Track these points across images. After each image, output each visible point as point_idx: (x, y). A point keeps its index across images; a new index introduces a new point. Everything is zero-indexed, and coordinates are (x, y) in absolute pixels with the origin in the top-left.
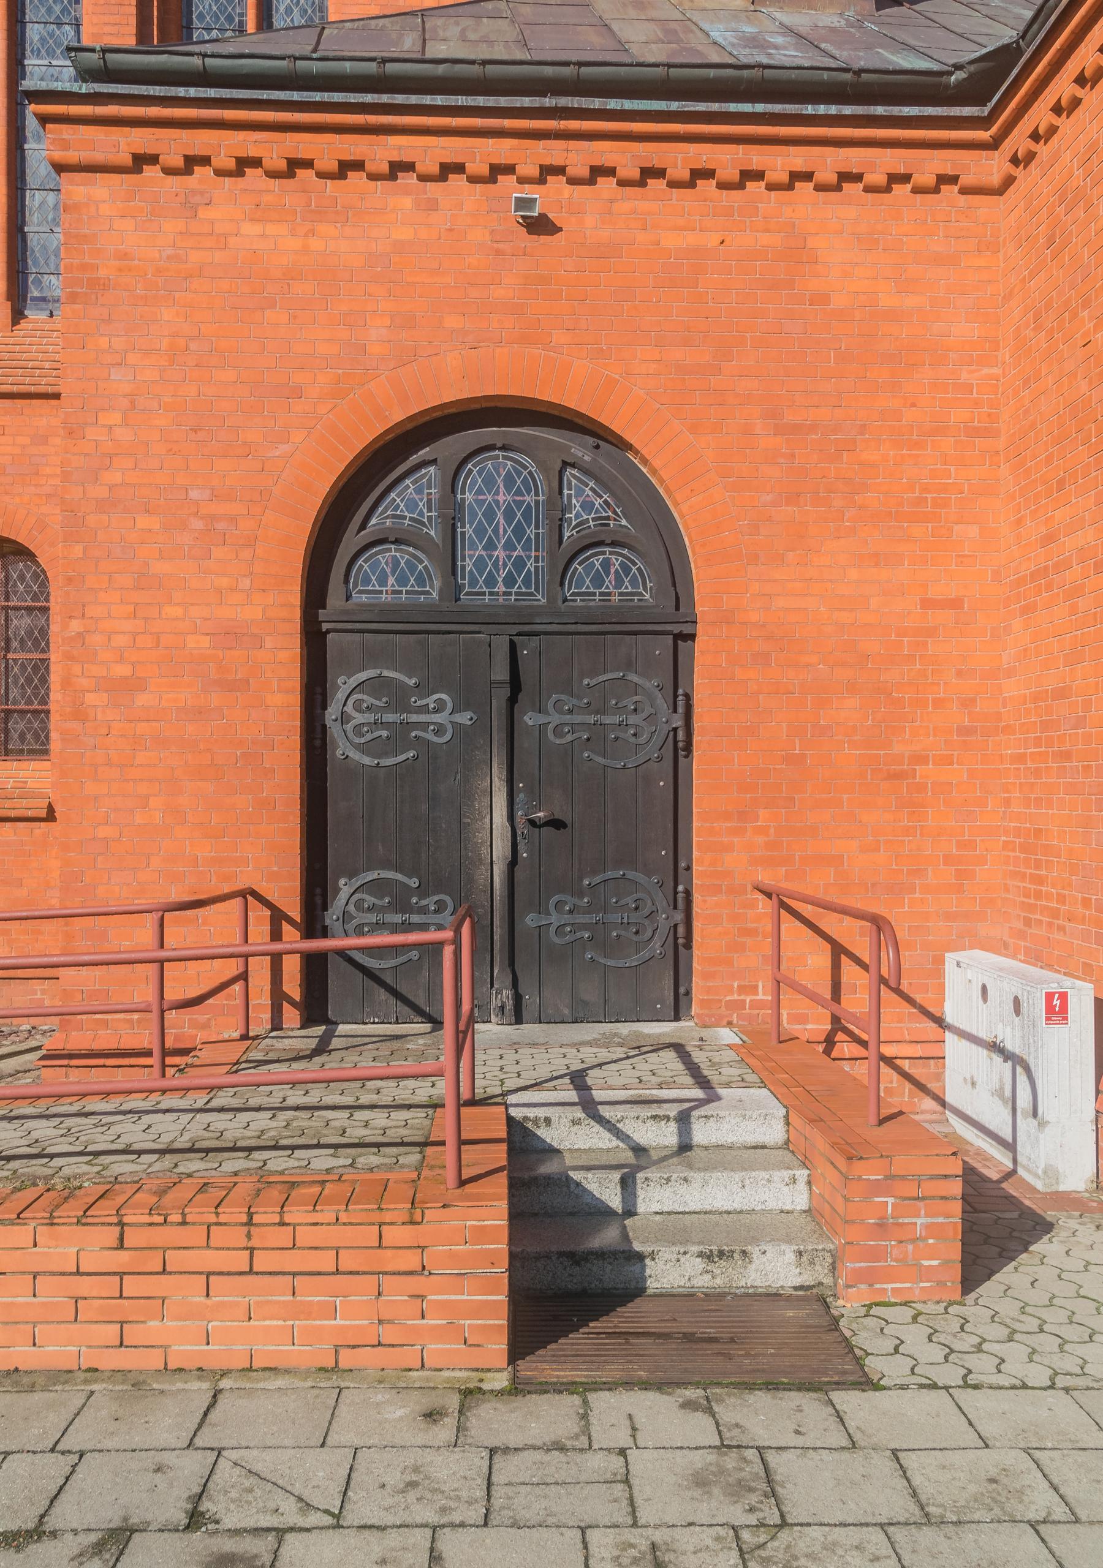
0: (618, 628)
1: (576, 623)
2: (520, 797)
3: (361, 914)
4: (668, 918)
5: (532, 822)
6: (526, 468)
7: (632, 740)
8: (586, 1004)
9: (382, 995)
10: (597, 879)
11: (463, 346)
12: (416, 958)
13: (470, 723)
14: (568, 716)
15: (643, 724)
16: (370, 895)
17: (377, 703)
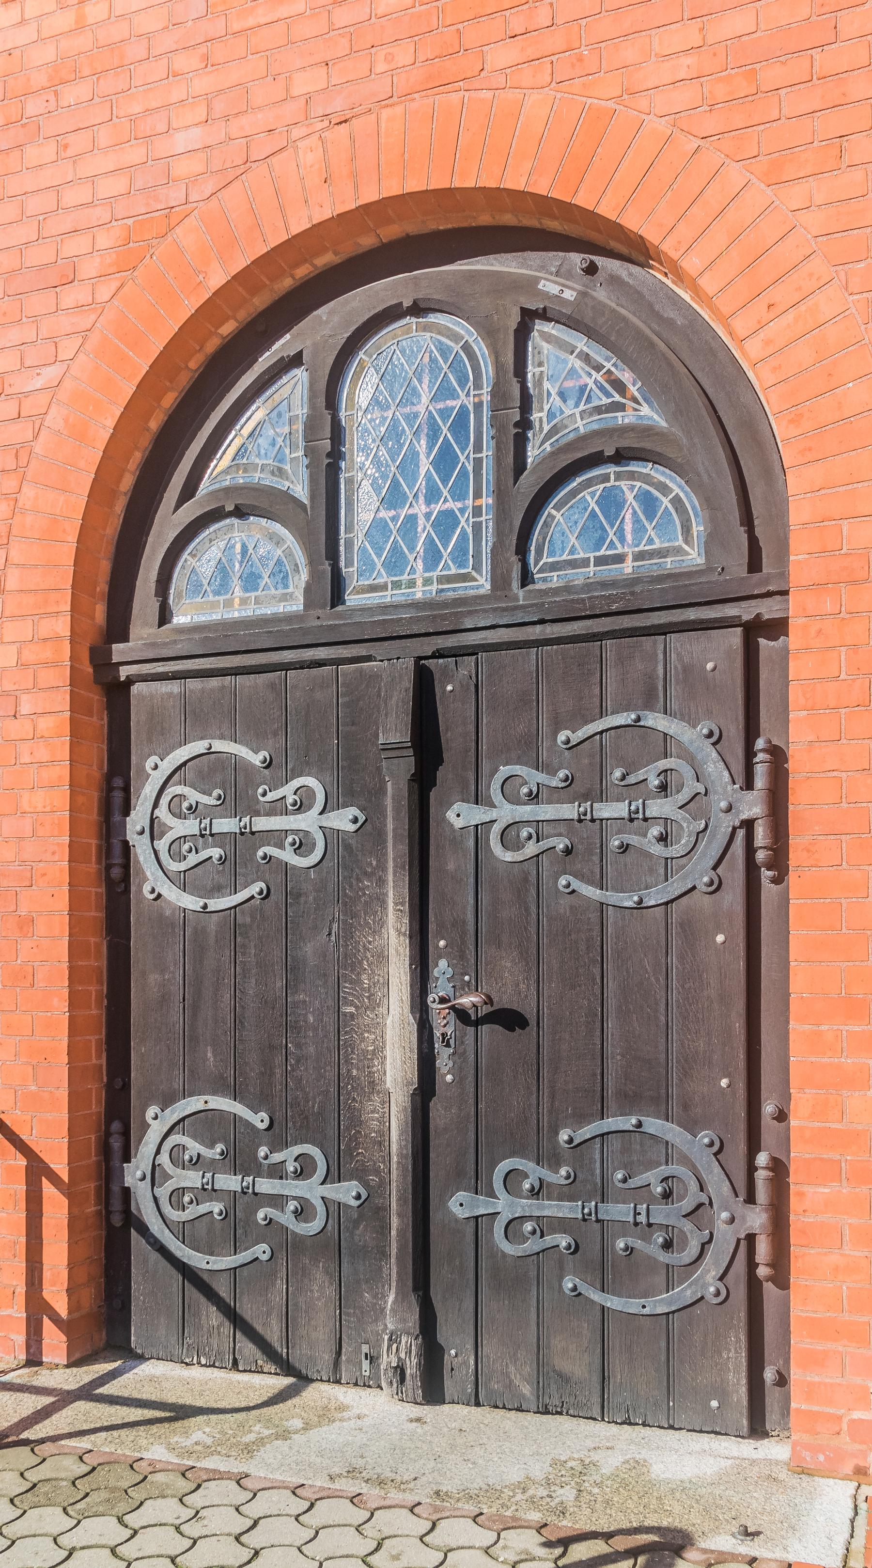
0: (627, 622)
1: (542, 622)
2: (441, 968)
3: (179, 1171)
4: (732, 1220)
5: (461, 1015)
6: (456, 337)
7: (657, 849)
8: (564, 1379)
9: (213, 1317)
10: (587, 1131)
11: (326, 123)
12: (265, 1257)
13: (352, 828)
14: (528, 808)
15: (679, 815)
16: (194, 1137)
17: (205, 800)
